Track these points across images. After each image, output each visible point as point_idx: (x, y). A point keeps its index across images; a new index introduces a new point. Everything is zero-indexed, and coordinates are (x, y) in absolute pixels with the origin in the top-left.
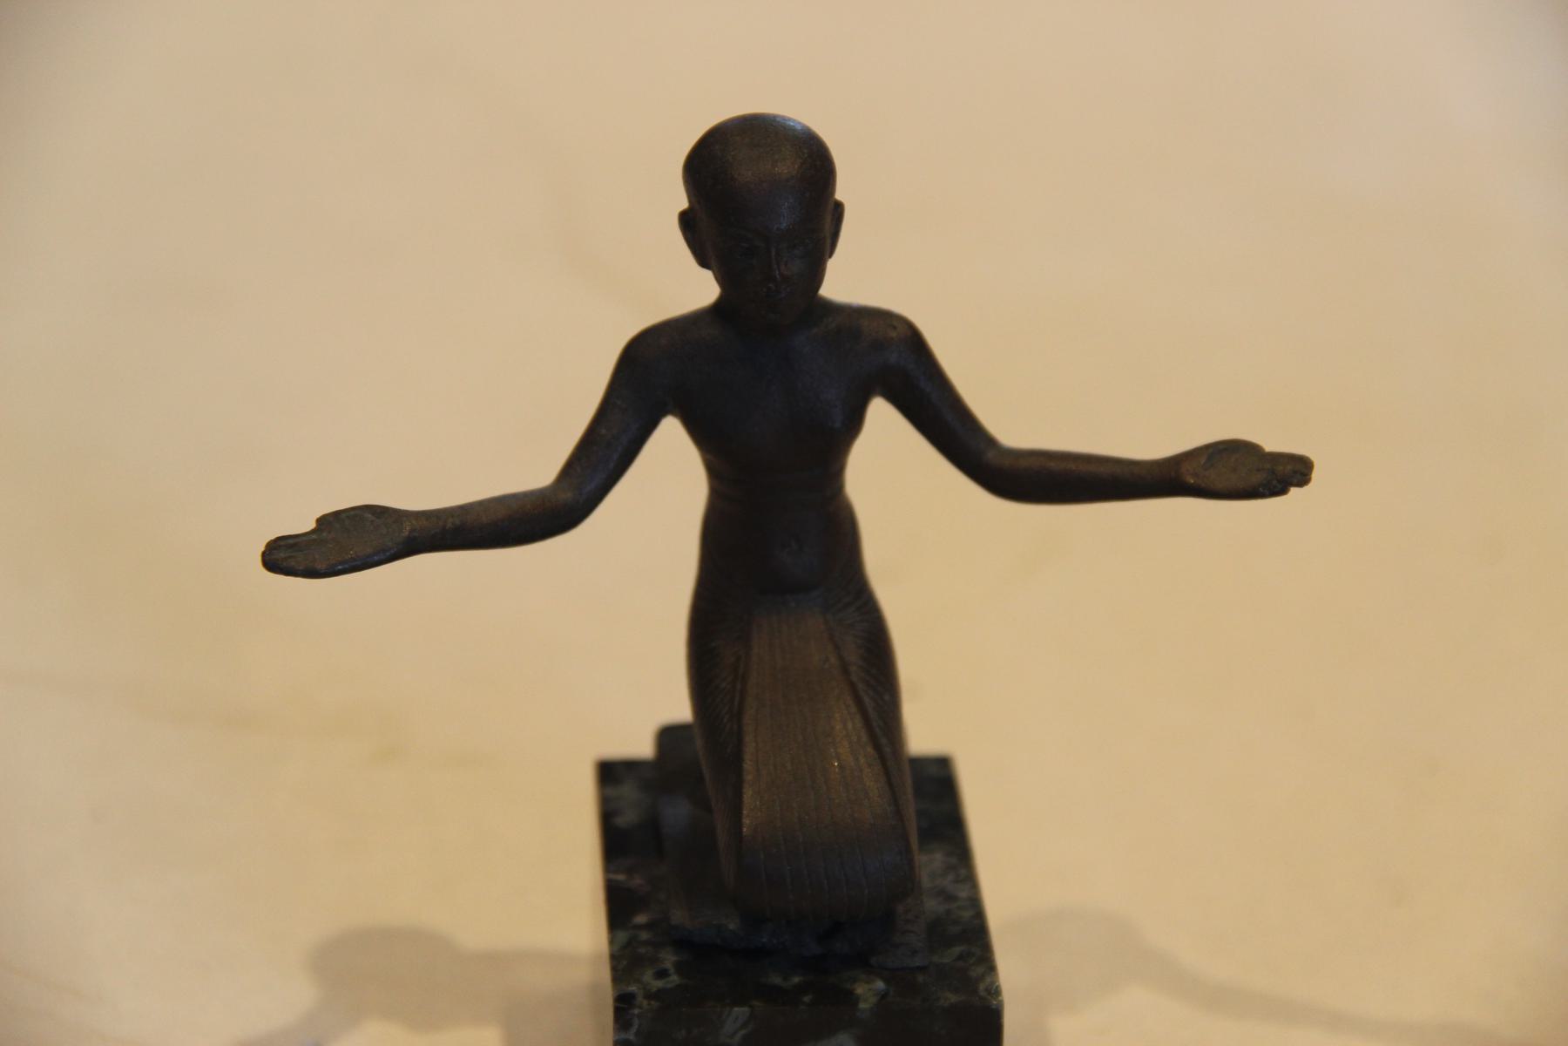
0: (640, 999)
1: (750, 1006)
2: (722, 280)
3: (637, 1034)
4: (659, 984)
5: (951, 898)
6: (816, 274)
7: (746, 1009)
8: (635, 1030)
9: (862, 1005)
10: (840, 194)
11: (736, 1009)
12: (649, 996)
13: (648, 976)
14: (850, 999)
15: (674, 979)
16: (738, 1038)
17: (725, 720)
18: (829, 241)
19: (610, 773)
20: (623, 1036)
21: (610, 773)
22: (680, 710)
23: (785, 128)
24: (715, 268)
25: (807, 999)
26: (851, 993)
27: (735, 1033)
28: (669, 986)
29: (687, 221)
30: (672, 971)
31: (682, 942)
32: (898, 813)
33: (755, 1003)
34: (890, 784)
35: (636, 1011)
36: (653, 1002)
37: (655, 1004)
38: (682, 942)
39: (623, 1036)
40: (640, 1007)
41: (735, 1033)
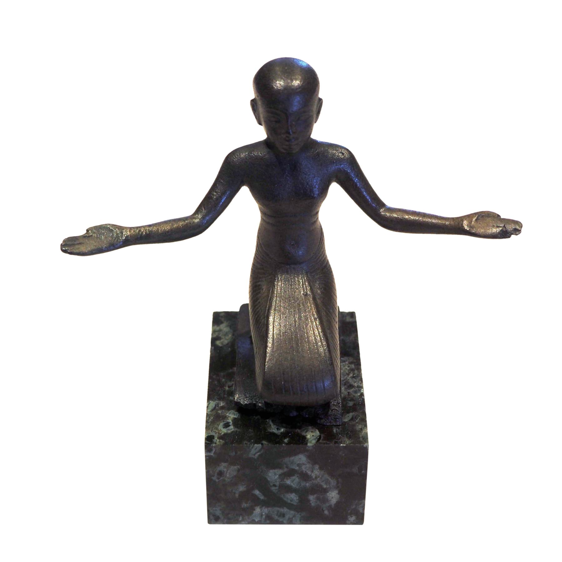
1: (262, 444)
2: (243, 185)
3: (214, 453)
4: (224, 431)
5: (351, 386)
6: (308, 126)
7: (260, 445)
8: (213, 452)
9: (309, 444)
10: (321, 95)
11: (256, 445)
12: (220, 438)
13: (221, 427)
14: (303, 440)
15: (232, 428)
16: (257, 455)
17: (261, 314)
18: (315, 116)
19: (218, 318)
20: (209, 454)
21: (218, 318)
22: (246, 299)
24: (263, 125)
25: (286, 440)
27: (256, 454)
28: (229, 432)
29: (254, 103)
30: (231, 424)
31: (240, 408)
32: (331, 358)
33: (264, 442)
35: (214, 445)
36: (221, 440)
37: (222, 442)
38: (240, 408)
39: (209, 454)
41: (256, 454)
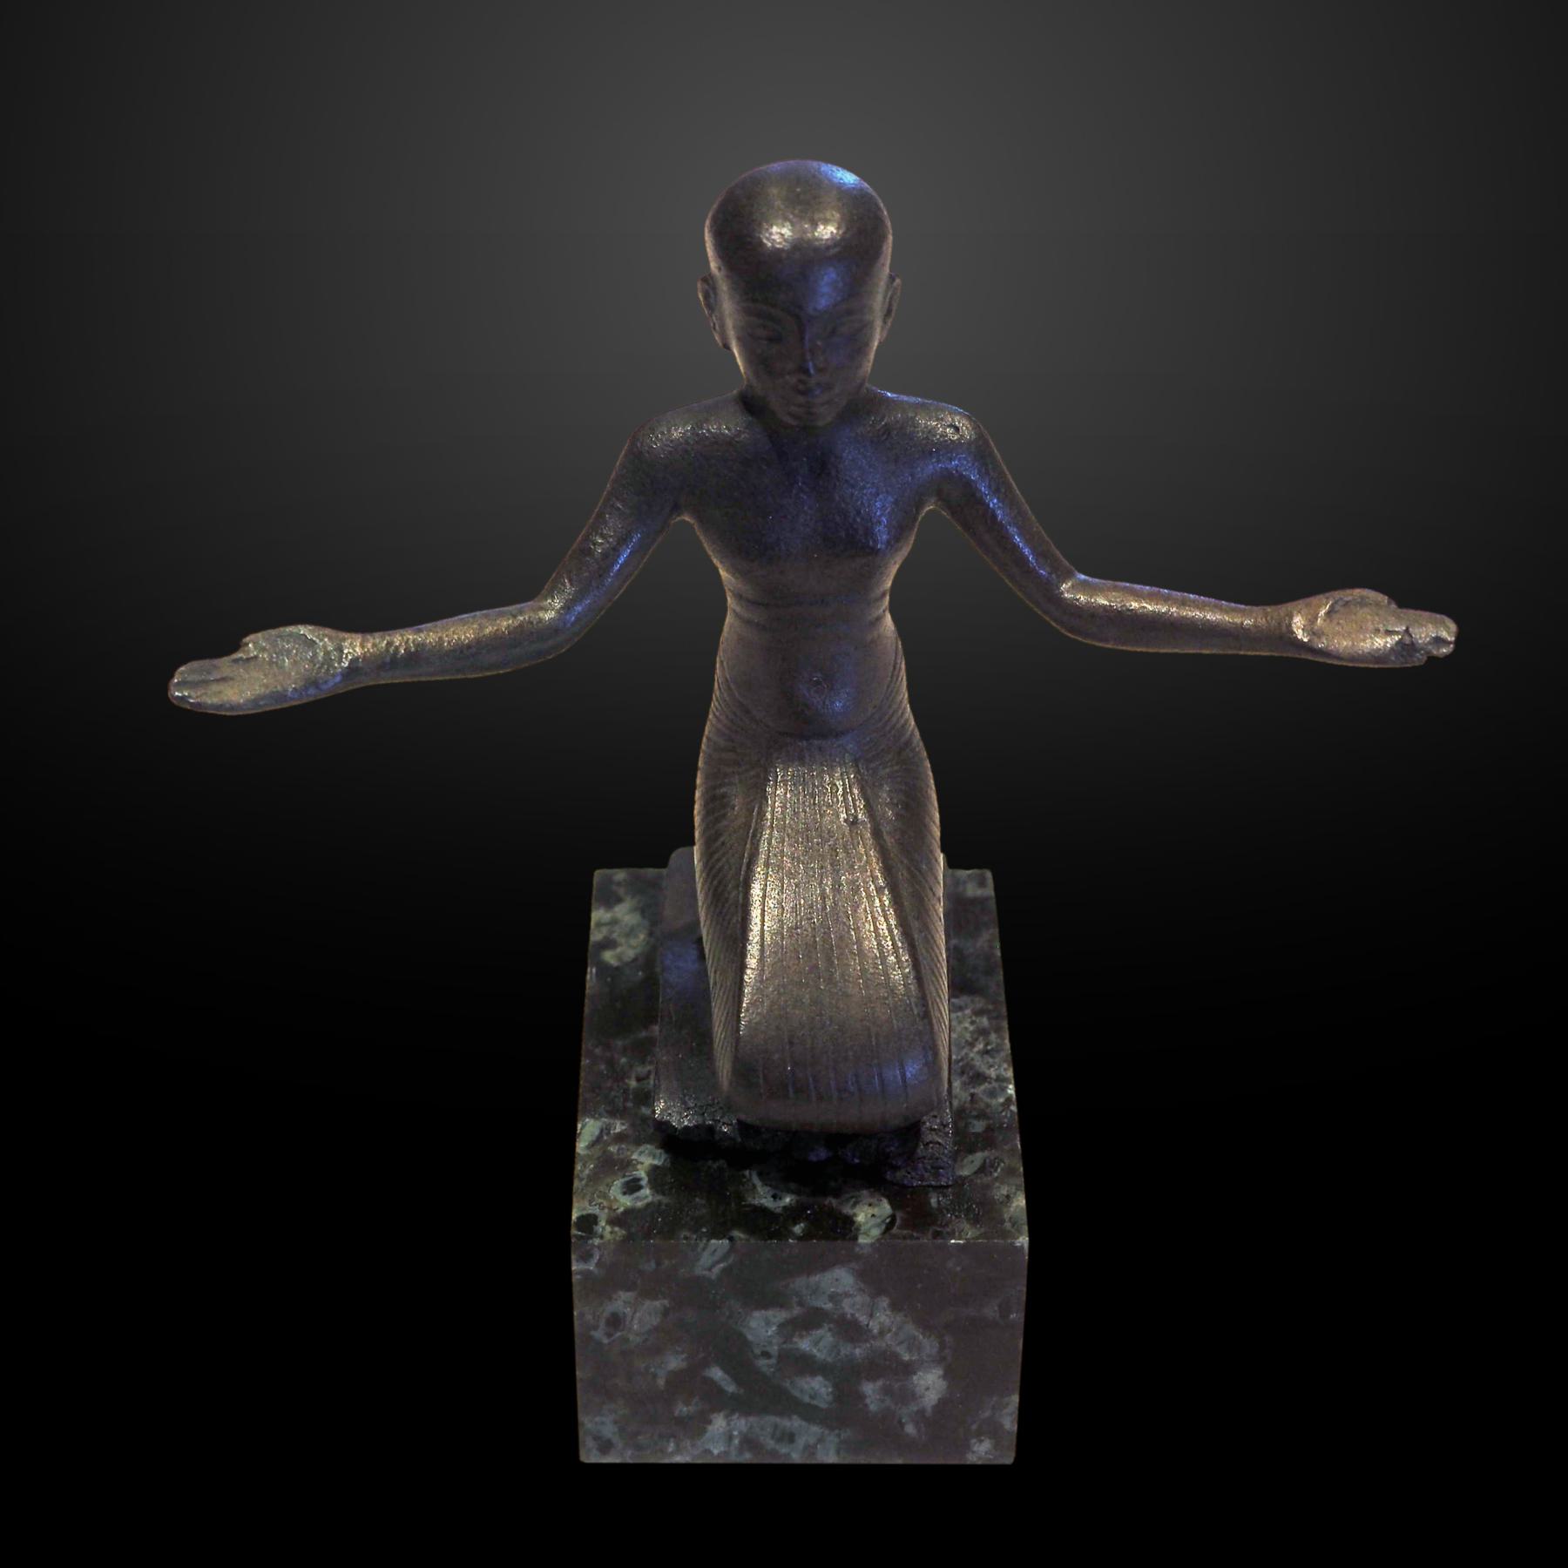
0: (603, 1227)
1: (731, 1239)
3: (598, 1264)
4: (626, 1202)
7: (726, 1242)
8: (596, 1261)
9: (862, 1240)
11: (713, 1241)
12: (614, 1221)
14: (845, 1228)
15: (646, 1194)
16: (716, 1270)
25: (798, 1229)
27: (713, 1265)
28: (639, 1204)
30: (644, 1182)
31: (669, 1139)
32: (923, 999)
33: (736, 1233)
34: (919, 979)
35: (597, 1241)
36: (617, 1229)
37: (620, 1232)
38: (669, 1139)
40: (602, 1237)
41: (713, 1265)
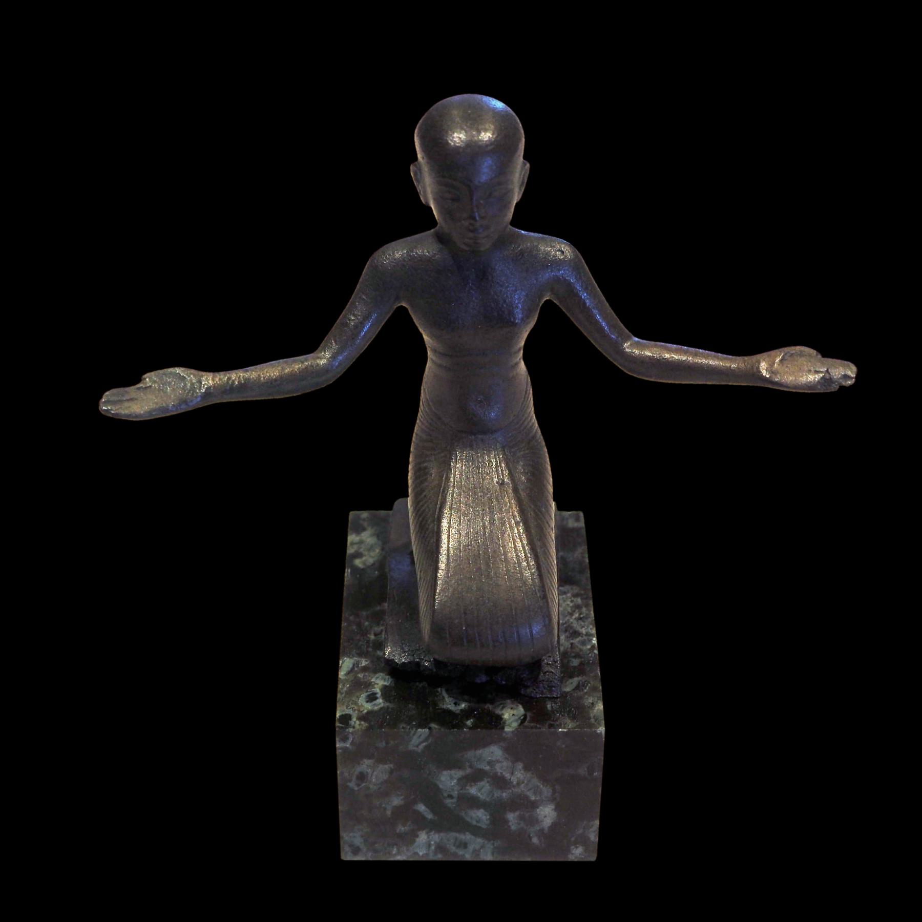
0: (354, 721)
1: (430, 729)
3: (352, 743)
4: (368, 707)
7: (427, 730)
8: (350, 742)
9: (507, 729)
11: (419, 730)
12: (361, 718)
14: (497, 722)
15: (380, 702)
16: (421, 747)
17: (429, 515)
23: (721, 370)
25: (469, 723)
26: (499, 718)
27: (419, 744)
28: (376, 708)
30: (379, 695)
32: (543, 587)
33: (433, 725)
34: (540, 576)
35: (351, 730)
36: (363, 723)
37: (365, 725)
40: (354, 727)
41: (419, 744)
